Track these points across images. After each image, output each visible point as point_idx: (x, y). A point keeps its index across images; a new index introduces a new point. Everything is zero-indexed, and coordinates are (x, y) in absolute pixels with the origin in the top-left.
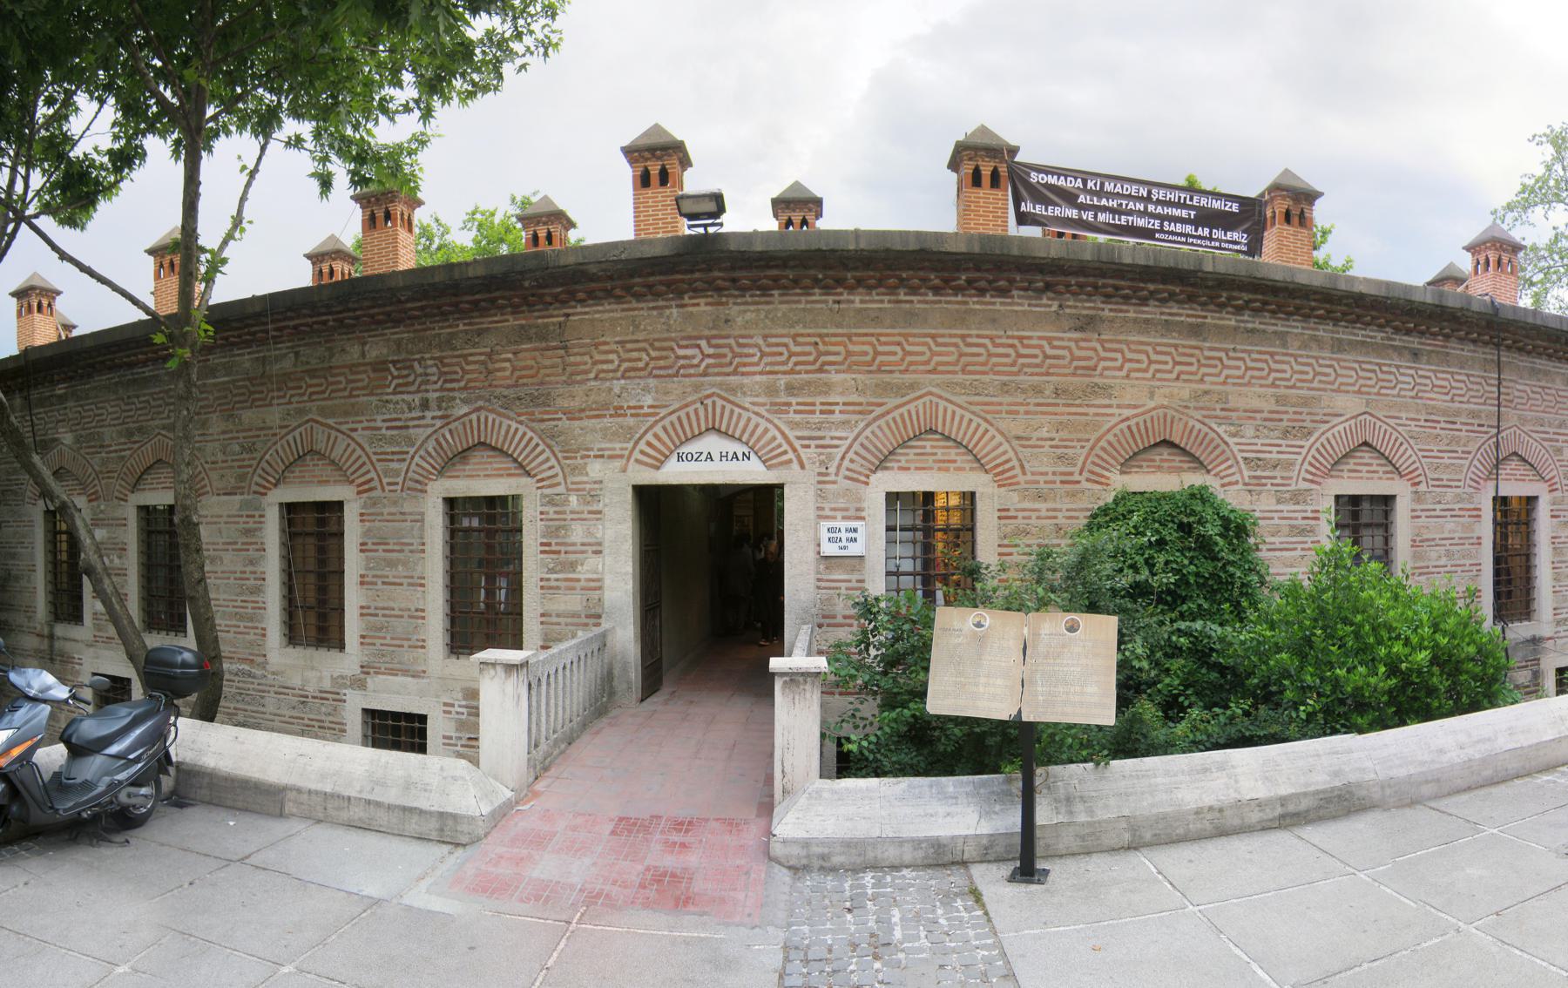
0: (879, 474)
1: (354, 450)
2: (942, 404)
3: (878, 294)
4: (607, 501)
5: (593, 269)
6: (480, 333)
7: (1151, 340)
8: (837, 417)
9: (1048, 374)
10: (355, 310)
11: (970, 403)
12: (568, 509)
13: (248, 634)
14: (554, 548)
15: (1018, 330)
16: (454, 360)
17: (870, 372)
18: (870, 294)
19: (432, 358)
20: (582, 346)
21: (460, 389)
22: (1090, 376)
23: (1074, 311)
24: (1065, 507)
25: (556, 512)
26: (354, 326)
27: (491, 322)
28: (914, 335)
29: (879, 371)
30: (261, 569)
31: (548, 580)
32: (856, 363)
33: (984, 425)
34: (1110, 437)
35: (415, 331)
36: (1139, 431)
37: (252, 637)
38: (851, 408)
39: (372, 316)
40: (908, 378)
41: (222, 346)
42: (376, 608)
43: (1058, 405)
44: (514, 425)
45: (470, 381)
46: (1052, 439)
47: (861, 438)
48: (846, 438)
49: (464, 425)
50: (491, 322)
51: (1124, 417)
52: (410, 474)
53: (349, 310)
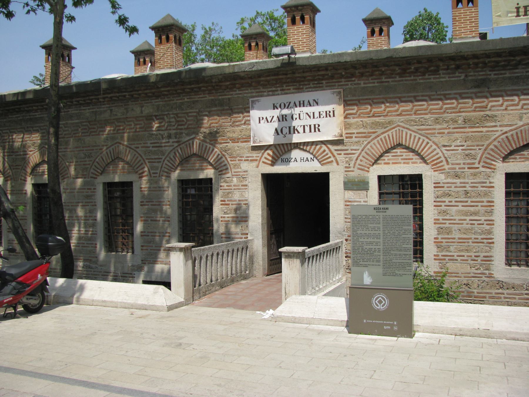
0: (375, 166)
1: (137, 158)
2: (405, 130)
3: (372, 79)
4: (250, 180)
5: (242, 75)
6: (194, 102)
7: (520, 88)
8: (354, 139)
9: (460, 112)
10: (138, 91)
11: (419, 130)
12: (232, 184)
13: (89, 247)
14: (227, 202)
15: (443, 91)
16: (183, 115)
17: (369, 117)
18: (368, 80)
19: (173, 114)
20: (239, 108)
21: (185, 129)
22: (483, 111)
23: (474, 78)
24: (470, 181)
25: (227, 186)
26: (138, 98)
27: (199, 98)
28: (390, 98)
29: (373, 116)
30: (94, 215)
31: (224, 217)
32: (362, 113)
33: (426, 140)
34: (496, 143)
35: (165, 101)
36: (513, 139)
37: (90, 248)
38: (360, 135)
39: (146, 94)
40: (388, 119)
41: (76, 105)
42: (148, 232)
43: (466, 128)
44: (209, 146)
45: (189, 125)
46: (463, 146)
47: (366, 150)
48: (358, 150)
49: (186, 146)
50: (199, 98)
51: (503, 131)
52: (163, 169)
53: (136, 91)
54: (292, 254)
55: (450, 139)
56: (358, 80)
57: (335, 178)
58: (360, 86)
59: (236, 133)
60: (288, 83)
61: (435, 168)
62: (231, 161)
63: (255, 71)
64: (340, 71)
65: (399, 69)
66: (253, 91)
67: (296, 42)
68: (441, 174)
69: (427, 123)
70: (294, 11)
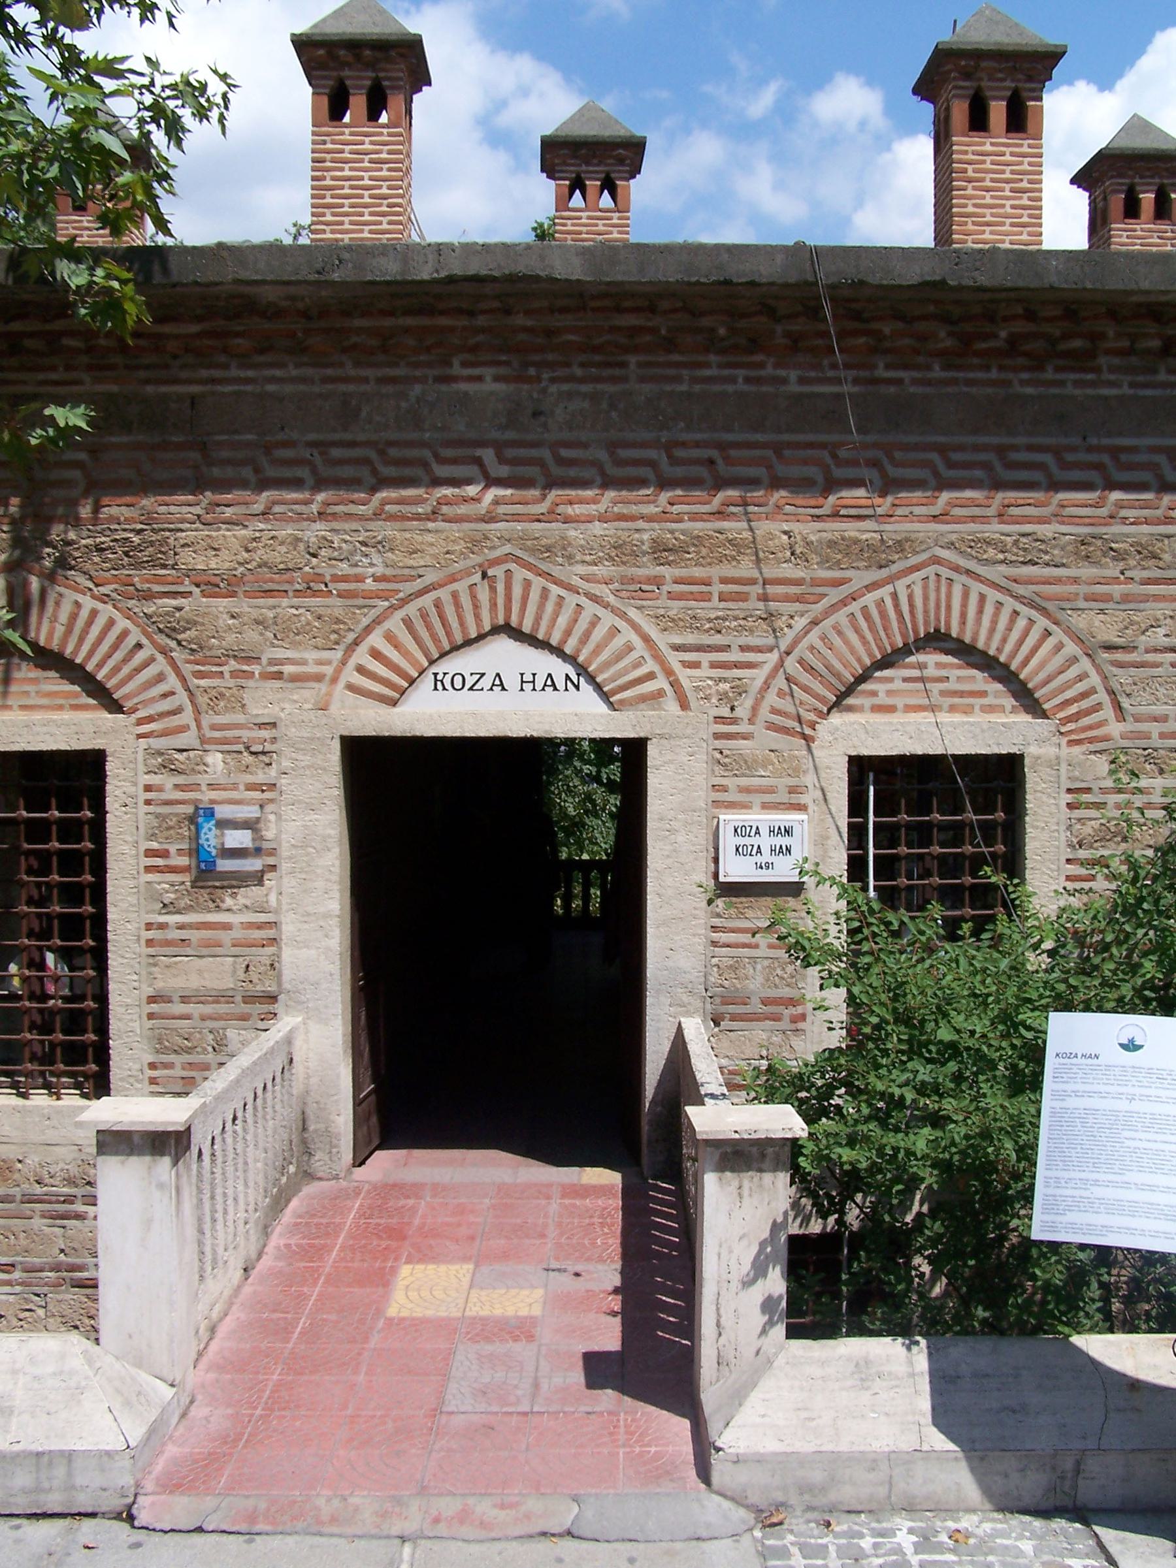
0: (836, 719)
5: (270, 294)
12: (203, 780)
17: (818, 518)
25: (177, 787)
28: (906, 448)
31: (162, 926)
47: (801, 650)
54: (754, 1150)
55: (1132, 623)
56: (777, 366)
57: (671, 762)
58: (783, 388)
59: (224, 554)
60: (474, 349)
61: (1071, 732)
62: (200, 675)
63: (343, 284)
64: (706, 322)
65: (950, 334)
66: (309, 372)
67: (347, 191)
68: (1092, 757)
69: (1047, 558)
70: (344, 65)
